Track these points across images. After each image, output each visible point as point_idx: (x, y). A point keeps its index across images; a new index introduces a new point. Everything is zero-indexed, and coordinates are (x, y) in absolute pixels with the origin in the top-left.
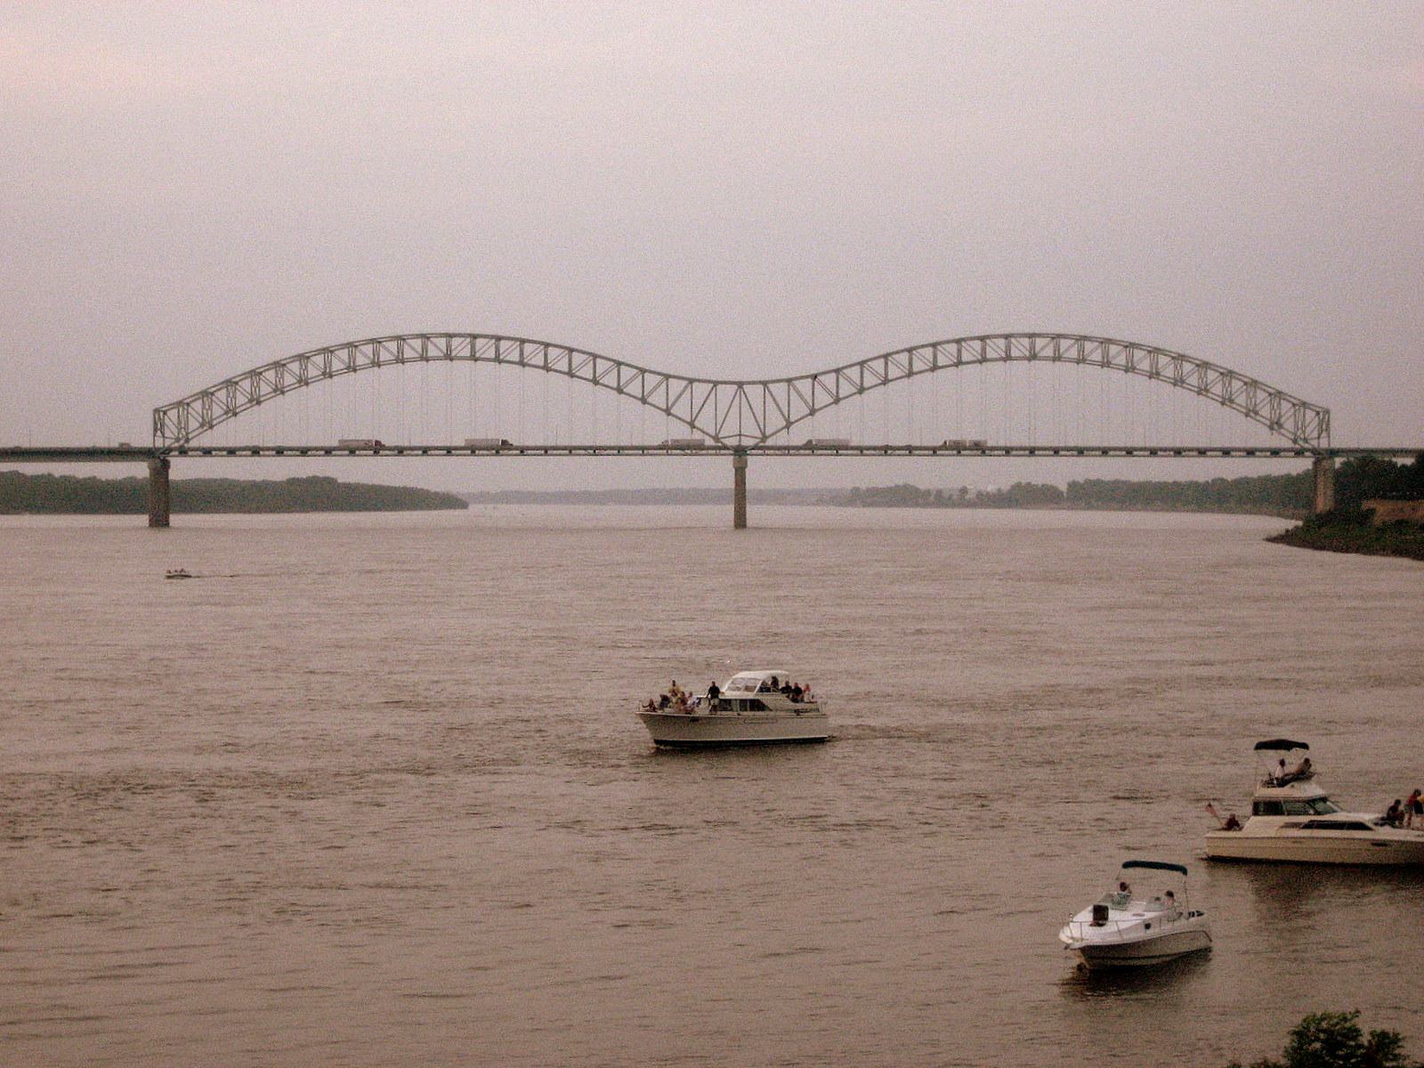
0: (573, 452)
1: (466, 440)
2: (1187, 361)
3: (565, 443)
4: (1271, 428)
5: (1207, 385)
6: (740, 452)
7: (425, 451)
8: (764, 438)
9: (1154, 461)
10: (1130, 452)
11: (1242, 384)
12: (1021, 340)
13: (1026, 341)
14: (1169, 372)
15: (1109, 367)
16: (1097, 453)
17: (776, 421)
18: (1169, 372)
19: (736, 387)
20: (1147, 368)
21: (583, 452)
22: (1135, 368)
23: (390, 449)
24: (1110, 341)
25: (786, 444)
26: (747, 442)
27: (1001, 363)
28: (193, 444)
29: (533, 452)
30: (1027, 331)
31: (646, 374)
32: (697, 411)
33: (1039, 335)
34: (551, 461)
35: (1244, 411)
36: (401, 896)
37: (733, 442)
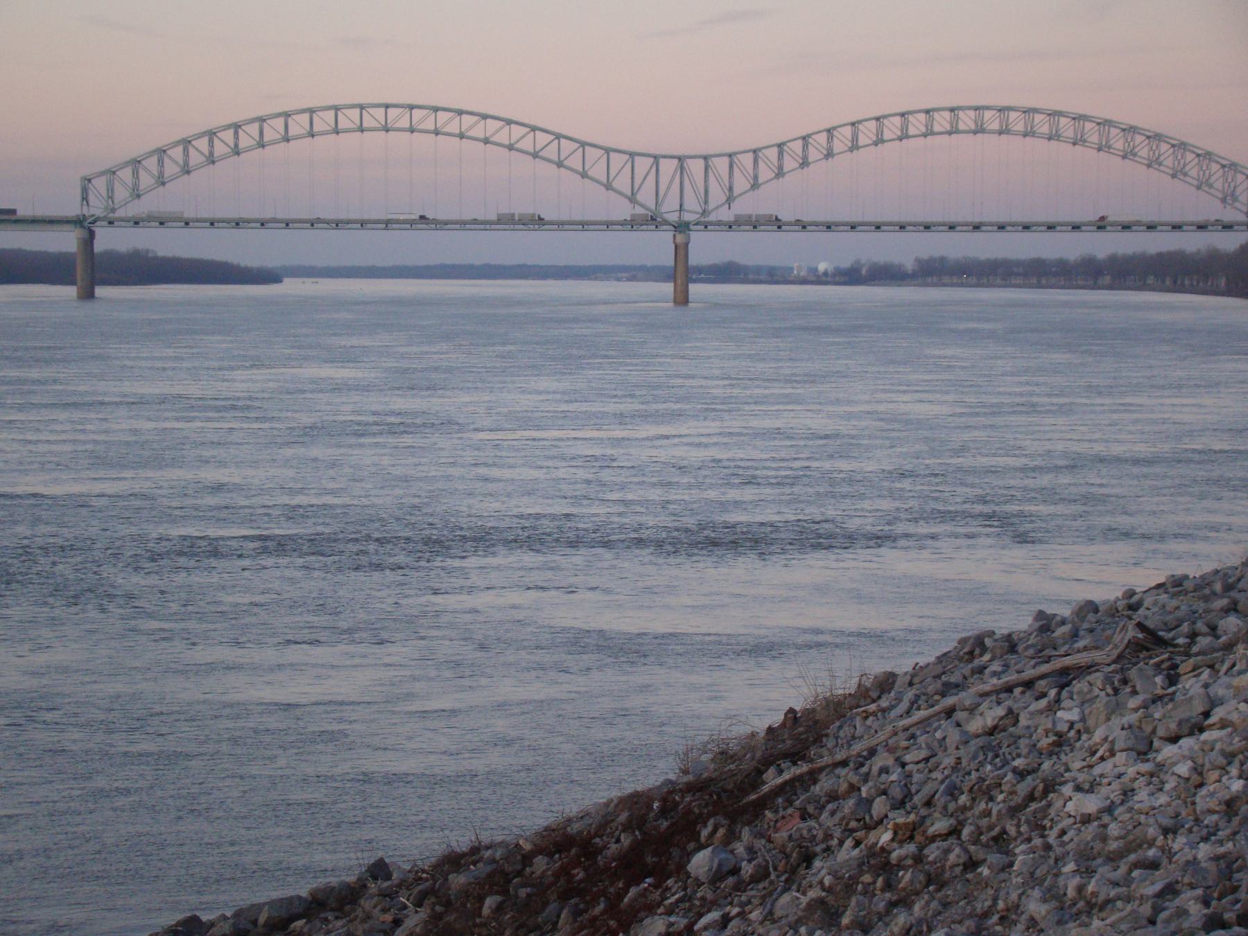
0: (291, 225)
1: (498, 215)
2: (1139, 134)
3: (579, 218)
4: (1224, 200)
5: (1185, 165)
6: (682, 227)
7: (363, 224)
8: (705, 213)
9: (1127, 235)
10: (1051, 227)
11: (1194, 156)
12: (967, 112)
13: (972, 113)
14: (1119, 144)
15: (1033, 136)
16: (846, 228)
17: (717, 195)
18: (1119, 144)
19: (603, 152)
20: (1071, 135)
21: (620, 227)
22: (1110, 147)
23: (551, 223)
24: (1060, 114)
25: (458, 218)
26: (687, 217)
27: (946, 136)
28: (120, 213)
29: (571, 227)
30: (974, 104)
31: (458, 132)
32: (639, 182)
33: (988, 108)
34: (394, 235)
35: (1195, 183)
36: (1024, 399)
37: (673, 217)
